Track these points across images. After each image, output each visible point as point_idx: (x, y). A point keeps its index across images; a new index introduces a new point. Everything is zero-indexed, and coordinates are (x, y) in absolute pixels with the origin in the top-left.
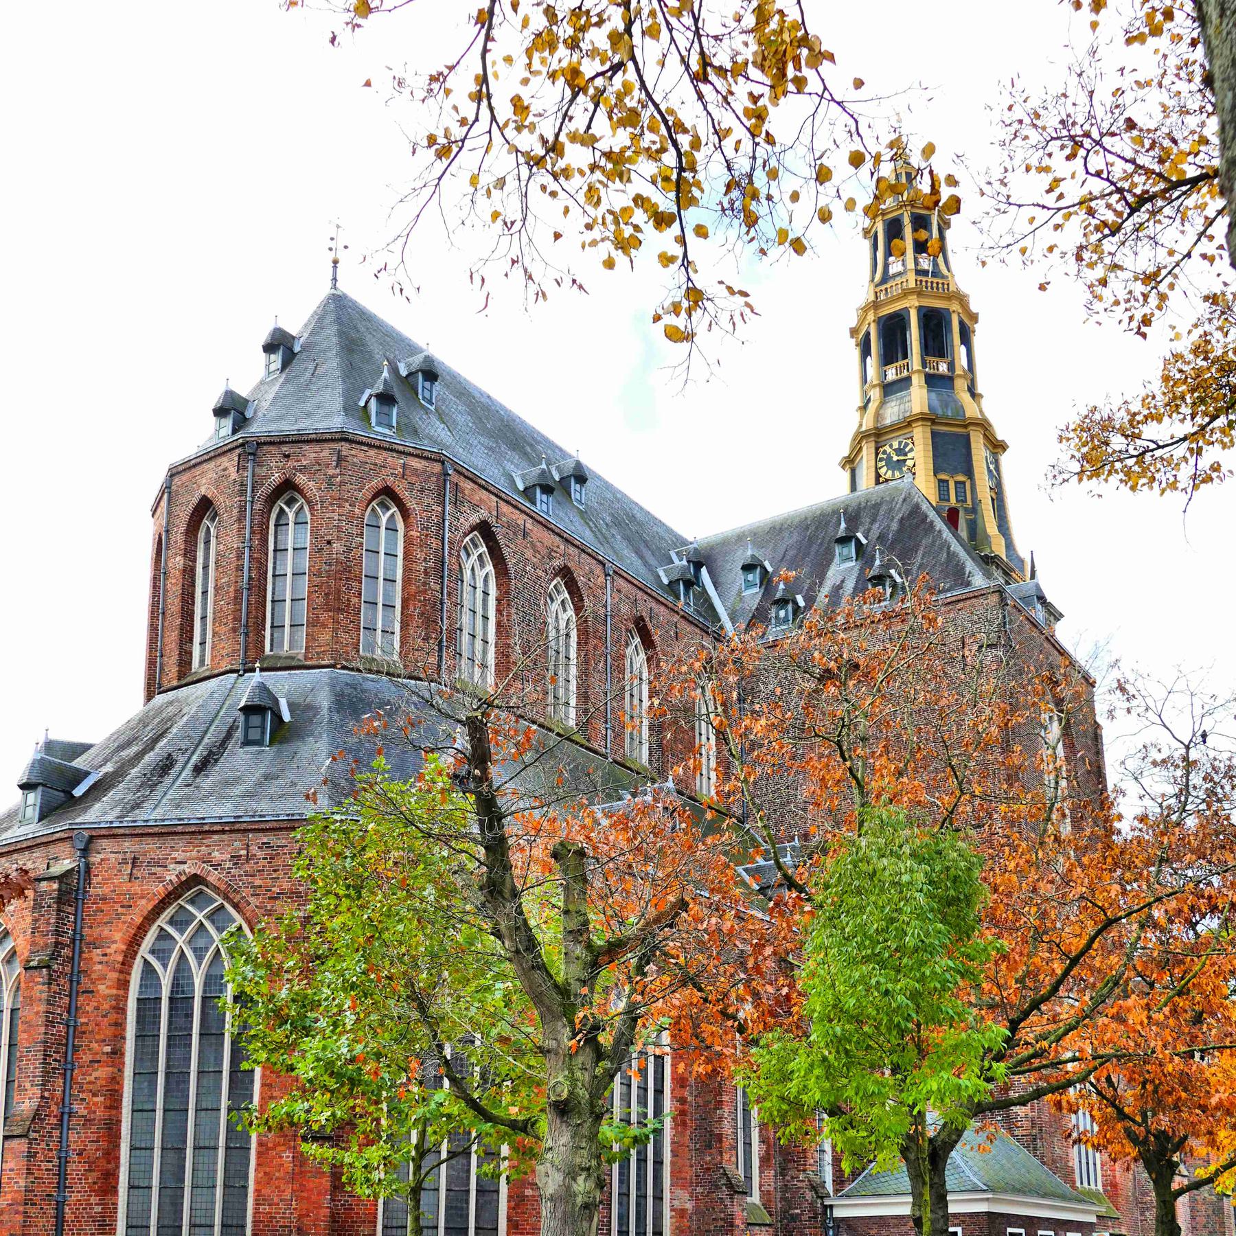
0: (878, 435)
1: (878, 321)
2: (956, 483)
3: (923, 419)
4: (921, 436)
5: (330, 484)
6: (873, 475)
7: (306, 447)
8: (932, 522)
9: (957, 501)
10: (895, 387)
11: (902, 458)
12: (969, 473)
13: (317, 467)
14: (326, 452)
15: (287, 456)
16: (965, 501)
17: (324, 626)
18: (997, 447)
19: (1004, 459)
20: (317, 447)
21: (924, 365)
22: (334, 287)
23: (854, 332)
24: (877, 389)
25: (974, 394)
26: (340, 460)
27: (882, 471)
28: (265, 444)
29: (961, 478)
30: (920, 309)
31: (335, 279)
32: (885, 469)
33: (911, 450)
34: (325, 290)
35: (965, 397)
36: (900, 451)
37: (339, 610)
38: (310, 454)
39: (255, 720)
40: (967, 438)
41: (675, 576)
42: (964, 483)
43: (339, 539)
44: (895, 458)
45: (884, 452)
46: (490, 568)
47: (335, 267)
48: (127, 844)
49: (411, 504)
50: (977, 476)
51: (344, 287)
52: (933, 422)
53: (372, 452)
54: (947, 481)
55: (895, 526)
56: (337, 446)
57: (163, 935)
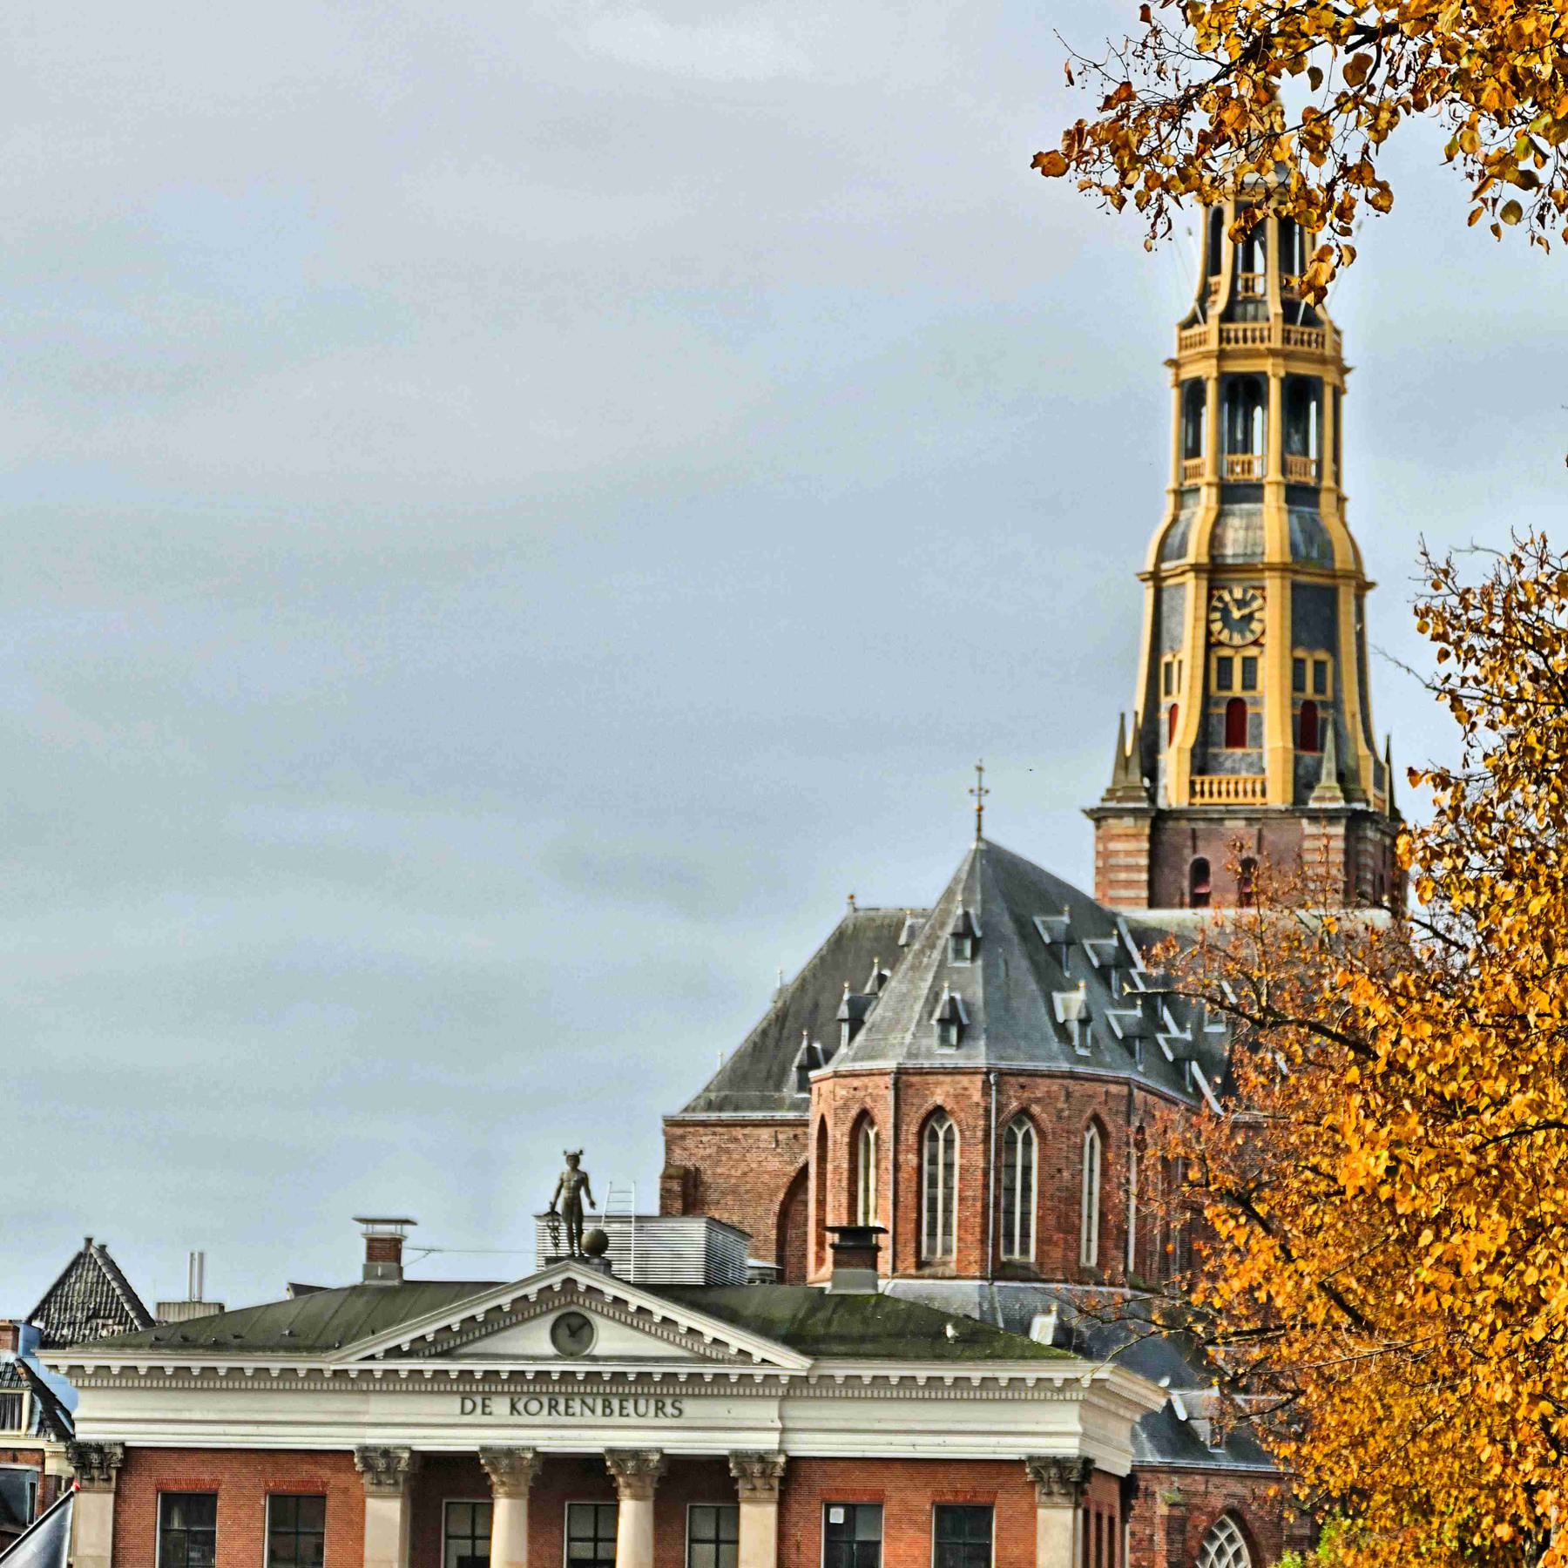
4: (1274, 586)
5: (1060, 1118)
6: (1202, 632)
7: (1039, 1080)
11: (1246, 611)
12: (1333, 647)
13: (1048, 1101)
14: (1055, 1085)
15: (1023, 1087)
17: (1056, 1244)
18: (1364, 586)
19: (1370, 597)
20: (1048, 1081)
22: (979, 838)
24: (1214, 491)
25: (1341, 500)
26: (1068, 1095)
27: (1217, 627)
28: (1007, 1074)
30: (1283, 381)
31: (979, 829)
33: (1261, 609)
36: (1241, 604)
38: (1042, 1087)
41: (1181, 1051)
43: (1068, 1168)
44: (1236, 614)
45: (1221, 599)
46: (1094, 1130)
47: (979, 816)
49: (1111, 1128)
50: (1343, 658)
51: (989, 833)
53: (1087, 1085)
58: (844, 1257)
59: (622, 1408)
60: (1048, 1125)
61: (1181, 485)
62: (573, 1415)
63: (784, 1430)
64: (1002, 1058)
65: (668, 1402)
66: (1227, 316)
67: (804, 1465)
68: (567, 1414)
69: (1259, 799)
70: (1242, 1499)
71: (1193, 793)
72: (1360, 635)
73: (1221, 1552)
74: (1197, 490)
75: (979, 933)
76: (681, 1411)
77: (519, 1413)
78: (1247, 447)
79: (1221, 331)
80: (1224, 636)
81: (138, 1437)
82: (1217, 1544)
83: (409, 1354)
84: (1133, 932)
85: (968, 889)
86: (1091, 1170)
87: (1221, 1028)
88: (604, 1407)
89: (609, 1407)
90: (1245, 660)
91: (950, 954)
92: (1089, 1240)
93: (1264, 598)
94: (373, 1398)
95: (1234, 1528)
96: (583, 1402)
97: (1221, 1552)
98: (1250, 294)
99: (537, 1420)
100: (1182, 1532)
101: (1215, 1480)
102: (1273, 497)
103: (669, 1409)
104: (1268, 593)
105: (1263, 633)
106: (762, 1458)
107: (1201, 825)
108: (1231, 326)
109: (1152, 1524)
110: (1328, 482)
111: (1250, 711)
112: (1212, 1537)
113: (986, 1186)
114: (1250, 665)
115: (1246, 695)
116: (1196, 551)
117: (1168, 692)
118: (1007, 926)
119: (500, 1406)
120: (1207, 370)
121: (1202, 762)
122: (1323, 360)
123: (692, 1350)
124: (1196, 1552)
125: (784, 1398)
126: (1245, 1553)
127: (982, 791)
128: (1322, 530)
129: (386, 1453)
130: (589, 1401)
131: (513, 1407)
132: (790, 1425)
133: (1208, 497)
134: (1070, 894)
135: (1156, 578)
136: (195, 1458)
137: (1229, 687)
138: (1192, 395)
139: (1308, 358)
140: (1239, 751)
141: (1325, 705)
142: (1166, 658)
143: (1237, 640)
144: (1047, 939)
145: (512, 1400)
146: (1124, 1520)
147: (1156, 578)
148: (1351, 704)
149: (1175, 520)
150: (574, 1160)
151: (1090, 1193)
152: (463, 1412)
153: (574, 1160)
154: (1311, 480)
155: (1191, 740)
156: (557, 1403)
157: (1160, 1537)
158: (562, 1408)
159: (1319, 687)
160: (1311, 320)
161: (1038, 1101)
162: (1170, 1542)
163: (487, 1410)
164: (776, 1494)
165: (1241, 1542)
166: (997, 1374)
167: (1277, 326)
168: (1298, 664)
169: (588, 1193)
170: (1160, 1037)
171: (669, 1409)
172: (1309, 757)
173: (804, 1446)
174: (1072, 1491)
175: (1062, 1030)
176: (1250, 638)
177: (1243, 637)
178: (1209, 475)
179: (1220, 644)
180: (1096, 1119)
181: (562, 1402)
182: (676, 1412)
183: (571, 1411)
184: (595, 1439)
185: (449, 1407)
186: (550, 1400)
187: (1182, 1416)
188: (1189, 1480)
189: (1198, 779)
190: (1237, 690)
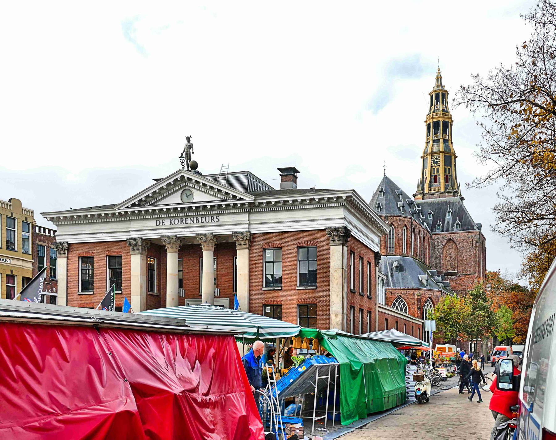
0: (432, 154)
1: (433, 122)
3: (443, 153)
4: (442, 156)
10: (436, 141)
12: (451, 166)
14: (398, 218)
16: (449, 173)
18: (456, 157)
19: (457, 159)
20: (396, 218)
22: (385, 175)
23: (425, 122)
24: (432, 141)
25: (452, 143)
26: (400, 220)
29: (449, 167)
30: (442, 121)
32: (433, 163)
33: (439, 159)
34: (383, 176)
35: (450, 145)
36: (436, 159)
37: (400, 246)
38: (395, 219)
39: (397, 268)
40: (451, 157)
44: (436, 161)
45: (433, 159)
46: (405, 227)
48: (391, 290)
49: (408, 227)
51: (387, 175)
52: (445, 153)
55: (457, 210)
56: (399, 218)
57: (394, 303)
58: (284, 178)
59: (202, 220)
60: (396, 226)
62: (188, 223)
63: (250, 224)
64: (388, 213)
65: (215, 217)
66: (434, 112)
67: (257, 236)
68: (186, 223)
69: (439, 191)
70: (431, 295)
71: (429, 191)
72: (455, 165)
73: (428, 306)
74: (429, 142)
75: (384, 192)
76: (219, 220)
77: (172, 224)
78: (437, 133)
80: (434, 165)
81: (72, 240)
82: (427, 304)
83: (139, 205)
84: (417, 204)
85: (383, 184)
86: (405, 235)
87: (431, 219)
88: (196, 220)
89: (198, 220)
91: (379, 196)
92: (404, 249)
94: (132, 222)
95: (430, 301)
96: (190, 219)
97: (428, 306)
99: (177, 226)
100: (420, 301)
101: (426, 291)
102: (441, 141)
103: (215, 220)
106: (242, 233)
107: (430, 196)
108: (434, 113)
109: (414, 299)
110: (450, 139)
111: (438, 177)
112: (426, 303)
113: (385, 238)
114: (438, 169)
115: (437, 174)
116: (429, 151)
118: (390, 191)
119: (167, 222)
120: (431, 121)
121: (430, 186)
122: (449, 118)
123: (221, 198)
124: (423, 305)
125: (250, 213)
126: (432, 305)
127: (385, 166)
128: (449, 147)
129: (135, 239)
130: (192, 219)
131: (171, 222)
132: (251, 222)
133: (431, 142)
134: (406, 197)
135: (423, 157)
136: (88, 245)
137: (435, 173)
138: (428, 126)
139: (447, 118)
140: (436, 184)
141: (449, 175)
142: (425, 170)
144: (397, 194)
145: (170, 220)
146: (376, 266)
147: (423, 157)
148: (454, 174)
149: (426, 148)
150: (188, 139)
151: (405, 240)
152: (157, 225)
153: (188, 139)
156: (183, 220)
157: (416, 302)
158: (184, 222)
159: (449, 173)
160: (447, 112)
161: (394, 221)
162: (418, 303)
163: (163, 224)
164: (248, 246)
165: (431, 303)
166: (315, 197)
167: (442, 112)
168: (445, 169)
169: (193, 150)
170: (420, 218)
171: (215, 220)
172: (447, 184)
173: (256, 229)
174: (342, 239)
175: (399, 208)
176: (438, 165)
180: (405, 225)
181: (184, 219)
182: (217, 220)
183: (187, 222)
184: (194, 231)
185: (152, 224)
186: (181, 219)
187: (421, 280)
188: (421, 291)
189: (430, 188)
190: (436, 174)
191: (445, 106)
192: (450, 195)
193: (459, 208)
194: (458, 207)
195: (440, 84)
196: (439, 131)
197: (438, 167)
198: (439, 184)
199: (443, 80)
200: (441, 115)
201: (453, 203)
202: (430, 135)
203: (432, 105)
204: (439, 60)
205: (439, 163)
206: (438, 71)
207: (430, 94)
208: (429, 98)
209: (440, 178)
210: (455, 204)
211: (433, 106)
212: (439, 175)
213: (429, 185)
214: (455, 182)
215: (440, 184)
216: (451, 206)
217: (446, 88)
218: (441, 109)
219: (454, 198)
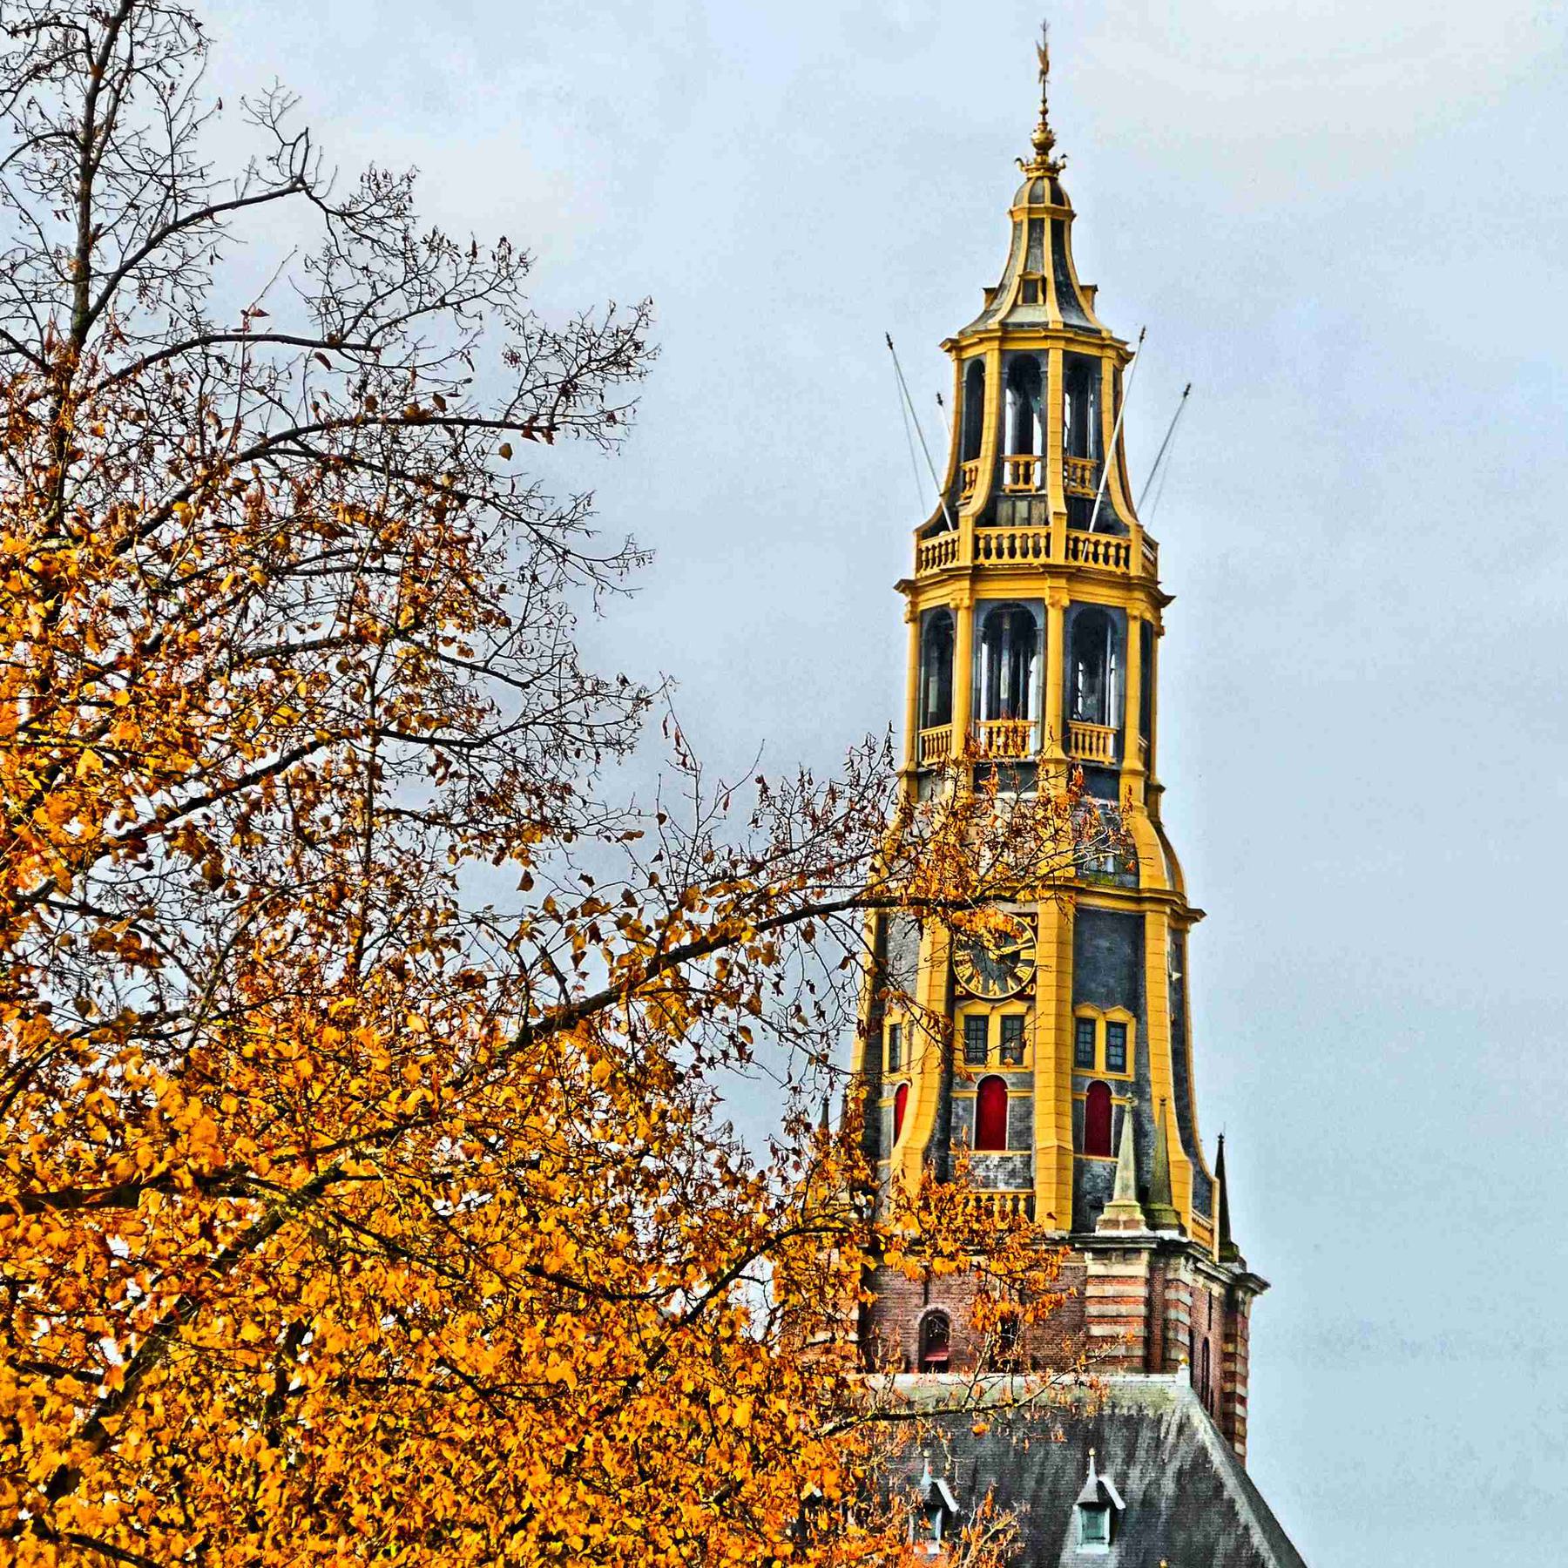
2: (1110, 1024)
4: (1048, 912)
6: (942, 977)
8: (1232, 1502)
9: (1110, 1067)
12: (1135, 1002)
16: (1122, 1069)
18: (1184, 917)
21: (1066, 747)
23: (906, 586)
25: (1153, 791)
40: (1138, 922)
42: (1123, 1026)
54: (1092, 1022)
55: (1169, 1486)
61: (919, 765)
66: (987, 517)
72: (1179, 989)
79: (976, 539)
90: (1005, 1018)
93: (1035, 929)
98: (1021, 486)
104: (1041, 922)
105: (1033, 980)
108: (993, 532)
110: (1132, 761)
111: (1012, 1094)
114: (1014, 1028)
115: (1007, 1074)
117: (894, 1069)
122: (1126, 583)
140: (995, 1156)
141: (1122, 1087)
142: (888, 1021)
143: (995, 990)
148: (1161, 1083)
154: (1107, 758)
155: (923, 1139)
167: (1059, 530)
172: (1098, 1163)
177: (1004, 989)
178: (956, 751)
179: (970, 996)
190: (994, 1066)
191: (1099, 469)
192: (1118, 1269)
193: (1180, 1473)
194: (1171, 1470)
195: (1049, 273)
196: (1034, 665)
197: (1018, 1008)
198: (1018, 1162)
199: (1078, 233)
200: (1058, 557)
201: (1133, 1423)
202: (944, 715)
203: (968, 444)
204: (1044, 56)
205: (1024, 972)
206: (1031, 154)
207: (954, 346)
208: (947, 375)
209: (1029, 1114)
210: (1146, 1435)
211: (983, 465)
212: (1028, 1082)
213: (926, 1158)
214: (1177, 1152)
215: (1027, 1163)
216: (1117, 1451)
217: (1107, 316)
218: (1056, 503)
219: (1140, 1377)
